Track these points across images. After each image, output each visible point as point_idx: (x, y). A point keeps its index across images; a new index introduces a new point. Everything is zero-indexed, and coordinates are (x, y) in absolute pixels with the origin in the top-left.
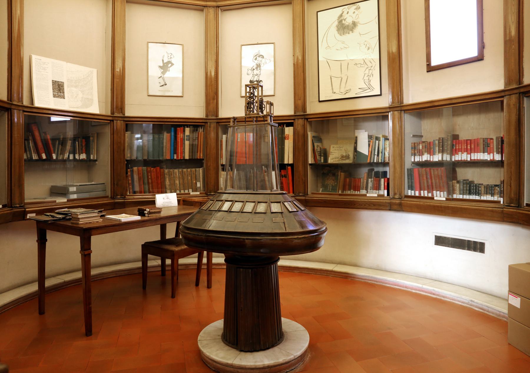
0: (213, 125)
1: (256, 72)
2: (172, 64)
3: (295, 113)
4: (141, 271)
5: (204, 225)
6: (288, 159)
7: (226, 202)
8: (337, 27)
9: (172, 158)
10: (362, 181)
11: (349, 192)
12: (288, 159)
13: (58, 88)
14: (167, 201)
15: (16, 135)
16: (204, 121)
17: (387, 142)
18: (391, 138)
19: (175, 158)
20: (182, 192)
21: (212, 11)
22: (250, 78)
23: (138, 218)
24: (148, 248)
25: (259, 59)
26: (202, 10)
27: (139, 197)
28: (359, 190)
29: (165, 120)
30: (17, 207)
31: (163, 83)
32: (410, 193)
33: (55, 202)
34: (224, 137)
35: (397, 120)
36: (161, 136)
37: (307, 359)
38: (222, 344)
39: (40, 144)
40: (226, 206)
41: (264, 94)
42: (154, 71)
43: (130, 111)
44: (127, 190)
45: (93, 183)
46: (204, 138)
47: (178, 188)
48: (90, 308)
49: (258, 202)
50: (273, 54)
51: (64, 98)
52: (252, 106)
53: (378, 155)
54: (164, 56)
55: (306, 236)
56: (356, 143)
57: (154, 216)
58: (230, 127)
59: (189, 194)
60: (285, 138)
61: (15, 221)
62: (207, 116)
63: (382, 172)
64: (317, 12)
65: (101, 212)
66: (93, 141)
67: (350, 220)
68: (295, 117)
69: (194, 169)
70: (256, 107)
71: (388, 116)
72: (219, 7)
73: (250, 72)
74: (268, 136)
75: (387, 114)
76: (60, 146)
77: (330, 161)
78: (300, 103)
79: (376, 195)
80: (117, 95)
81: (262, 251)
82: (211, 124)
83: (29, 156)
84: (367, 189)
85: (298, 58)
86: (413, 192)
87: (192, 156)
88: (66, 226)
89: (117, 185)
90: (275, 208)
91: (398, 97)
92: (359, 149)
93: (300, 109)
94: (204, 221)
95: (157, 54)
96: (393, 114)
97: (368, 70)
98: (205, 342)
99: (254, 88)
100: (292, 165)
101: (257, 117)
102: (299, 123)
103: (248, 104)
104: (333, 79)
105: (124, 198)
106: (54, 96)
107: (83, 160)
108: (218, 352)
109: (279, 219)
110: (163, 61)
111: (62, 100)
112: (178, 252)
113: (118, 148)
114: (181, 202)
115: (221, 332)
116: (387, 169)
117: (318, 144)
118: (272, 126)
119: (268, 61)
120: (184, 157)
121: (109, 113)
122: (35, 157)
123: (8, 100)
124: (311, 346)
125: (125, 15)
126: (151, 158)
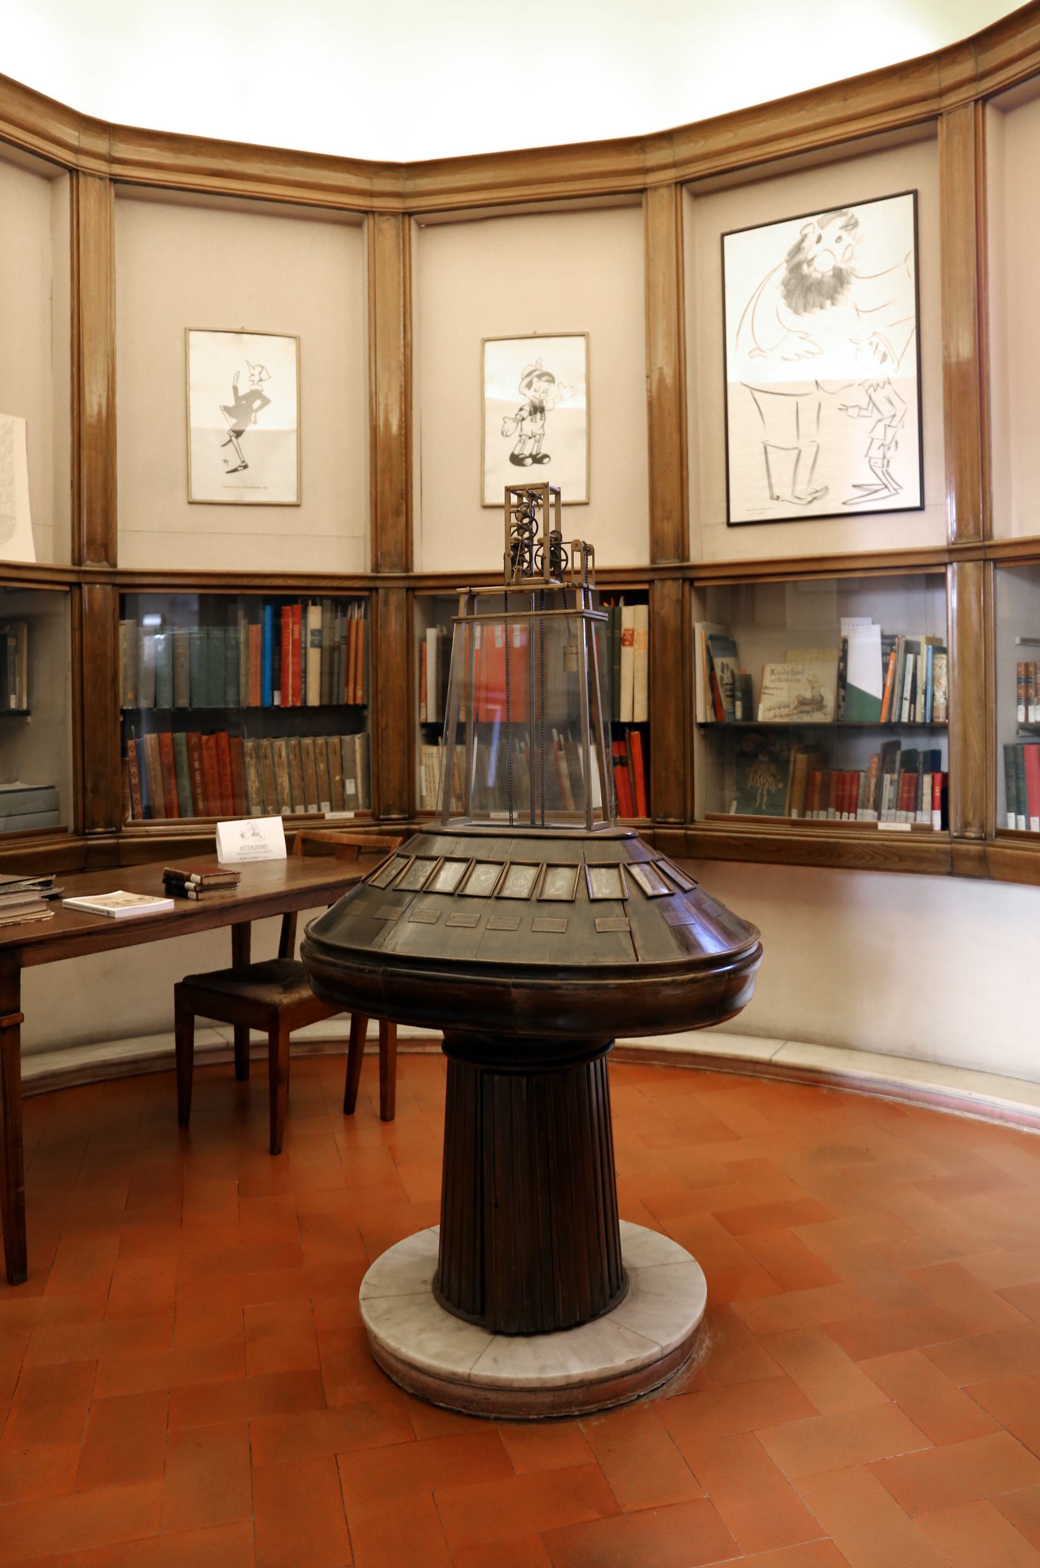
0: (396, 599)
1: (530, 426)
2: (266, 401)
3: (653, 560)
4: (173, 1064)
5: (379, 939)
6: (634, 706)
7: (448, 865)
8: (786, 284)
9: (267, 704)
10: (862, 780)
11: (822, 816)
12: (634, 706)
14: (252, 843)
17: (942, 660)
18: (953, 647)
19: (277, 702)
20: (300, 810)
21: (388, 227)
23: (165, 905)
24: (196, 996)
25: (539, 384)
26: (358, 225)
27: (160, 830)
28: (852, 809)
29: (245, 582)
31: (235, 463)
32: (1014, 822)
34: (432, 634)
35: (972, 590)
36: (231, 633)
37: (701, 1354)
38: (437, 1309)
40: (448, 877)
41: (563, 510)
42: (208, 417)
43: (136, 554)
44: (124, 808)
45: (18, 785)
46: (366, 638)
48: (20, 1197)
49: (550, 866)
52: (527, 556)
53: (913, 700)
55: (701, 975)
56: (844, 658)
57: (214, 899)
58: (459, 621)
59: (322, 817)
62: (376, 567)
63: (926, 754)
64: (723, 235)
65: (47, 884)
66: (17, 649)
67: (826, 901)
68: (653, 573)
69: (335, 740)
71: (944, 576)
72: (410, 214)
73: (511, 426)
75: (942, 570)
77: (764, 715)
78: (668, 528)
79: (907, 827)
81: (560, 1022)
82: (391, 595)
84: (877, 807)
85: (661, 380)
86: (1022, 818)
87: (331, 694)
89: (95, 791)
90: (603, 884)
91: (976, 518)
92: (853, 679)
94: (380, 926)
95: (216, 367)
96: (961, 570)
97: (881, 425)
98: (383, 1304)
100: (643, 728)
102: (667, 592)
103: (515, 547)
104: (769, 449)
105: (117, 833)
108: (425, 1336)
109: (614, 920)
110: (235, 389)
112: (289, 1007)
113: (96, 672)
114: (298, 845)
115: (430, 1271)
116: (942, 744)
117: (726, 660)
118: (589, 620)
120: (305, 700)
121: (66, 562)
124: (714, 1312)
125: (110, 245)
126: (200, 704)
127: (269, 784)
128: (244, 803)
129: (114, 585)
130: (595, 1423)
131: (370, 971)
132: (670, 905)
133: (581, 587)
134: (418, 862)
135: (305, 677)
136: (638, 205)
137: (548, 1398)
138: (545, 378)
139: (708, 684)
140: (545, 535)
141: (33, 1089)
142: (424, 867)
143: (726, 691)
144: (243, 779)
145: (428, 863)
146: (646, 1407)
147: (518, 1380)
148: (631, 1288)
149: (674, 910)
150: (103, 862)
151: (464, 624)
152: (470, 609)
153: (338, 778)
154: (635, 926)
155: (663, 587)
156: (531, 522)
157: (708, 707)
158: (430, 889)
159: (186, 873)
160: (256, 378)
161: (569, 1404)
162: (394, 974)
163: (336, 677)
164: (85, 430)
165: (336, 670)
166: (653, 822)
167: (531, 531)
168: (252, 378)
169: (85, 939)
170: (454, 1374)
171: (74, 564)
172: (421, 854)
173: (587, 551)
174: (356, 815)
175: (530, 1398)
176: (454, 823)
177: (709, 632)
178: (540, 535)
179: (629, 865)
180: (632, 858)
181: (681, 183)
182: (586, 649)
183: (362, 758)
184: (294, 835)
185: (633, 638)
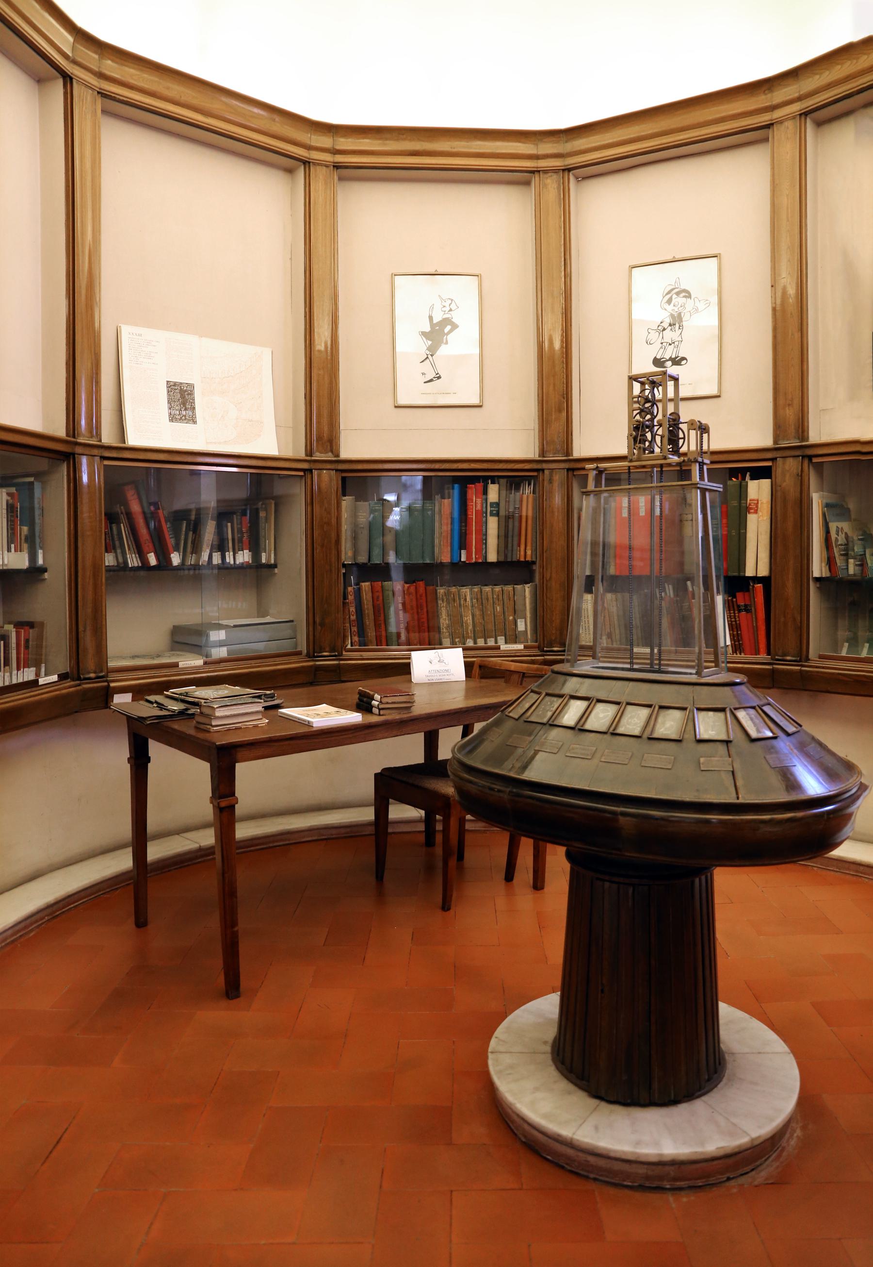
0: (559, 478)
1: (669, 335)
2: (455, 326)
3: (775, 442)
4: (371, 830)
6: (757, 562)
9: (456, 560)
12: (757, 562)
13: (182, 400)
14: (439, 669)
15: (86, 515)
16: (535, 466)
20: (481, 642)
22: (655, 351)
23: (354, 717)
24: (391, 784)
25: (679, 300)
26: (527, 183)
30: (90, 679)
33: (176, 665)
38: (552, 1071)
39: (143, 531)
40: (572, 713)
42: (410, 343)
43: (355, 446)
47: (471, 634)
50: (715, 285)
51: (195, 422)
52: (649, 436)
54: (432, 308)
55: (799, 814)
59: (498, 648)
60: (747, 510)
61: (85, 710)
62: (542, 452)
66: (267, 519)
68: (776, 451)
69: (509, 588)
70: (658, 439)
72: (569, 170)
73: (654, 336)
74: (694, 520)
76: (191, 533)
78: (790, 414)
80: (319, 408)
82: (553, 471)
83: (121, 560)
88: (186, 731)
90: (709, 726)
93: (792, 430)
95: (415, 304)
98: (507, 1059)
99: (654, 384)
100: (765, 581)
101: (661, 466)
102: (788, 468)
103: (636, 428)
105: (339, 657)
106: (172, 419)
107: (242, 567)
108: (539, 1095)
109: (718, 760)
110: (431, 318)
111: (189, 426)
113: (322, 539)
114: (476, 670)
115: (551, 1033)
117: (840, 524)
118: (704, 491)
119: (701, 306)
121: (302, 454)
122: (133, 561)
123: (67, 435)
127: (457, 620)
128: (437, 636)
129: (337, 470)
130: (685, 1200)
131: (499, 791)
132: (773, 747)
133: (696, 461)
134: (548, 698)
135: (486, 540)
136: (766, 140)
137: (642, 1170)
138: (682, 295)
139: (824, 545)
140: (664, 416)
141: (274, 842)
142: (552, 703)
143: (840, 550)
144: (437, 616)
145: (555, 699)
146: (735, 1190)
147: (615, 1151)
148: (728, 1072)
149: (777, 752)
150: (314, 681)
151: (592, 496)
152: (598, 483)
153: (511, 618)
154: (737, 766)
155: (784, 464)
156: (652, 406)
157: (823, 565)
158: (555, 723)
159: (372, 693)
160: (447, 309)
161: (661, 1178)
162: (518, 795)
163: (510, 540)
164: (315, 355)
165: (510, 534)
166: (772, 659)
167: (652, 414)
168: (444, 309)
169: (287, 742)
170: (559, 1135)
171: (307, 455)
172: (550, 692)
173: (703, 429)
174: (525, 647)
175: (626, 1167)
176: (581, 665)
177: (825, 501)
178: (660, 417)
179: (736, 709)
180: (740, 703)
181: (805, 114)
182: (700, 517)
183: (531, 603)
184: (473, 663)
185: (757, 507)
